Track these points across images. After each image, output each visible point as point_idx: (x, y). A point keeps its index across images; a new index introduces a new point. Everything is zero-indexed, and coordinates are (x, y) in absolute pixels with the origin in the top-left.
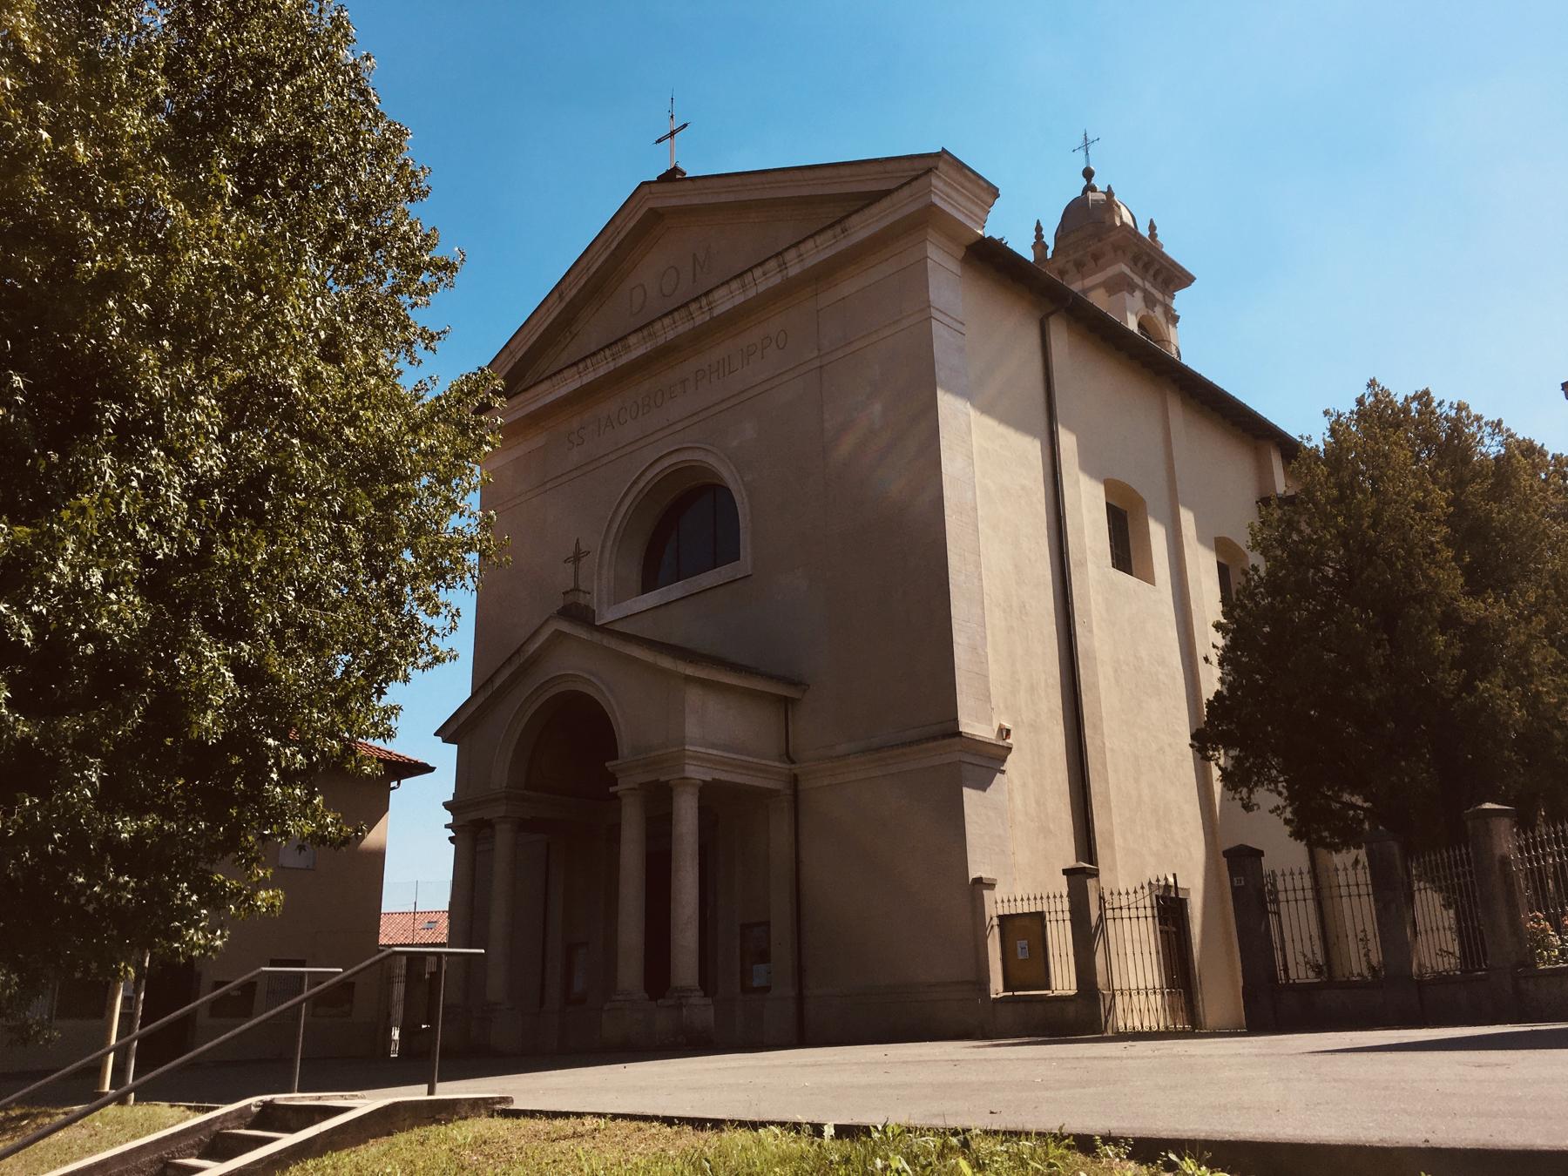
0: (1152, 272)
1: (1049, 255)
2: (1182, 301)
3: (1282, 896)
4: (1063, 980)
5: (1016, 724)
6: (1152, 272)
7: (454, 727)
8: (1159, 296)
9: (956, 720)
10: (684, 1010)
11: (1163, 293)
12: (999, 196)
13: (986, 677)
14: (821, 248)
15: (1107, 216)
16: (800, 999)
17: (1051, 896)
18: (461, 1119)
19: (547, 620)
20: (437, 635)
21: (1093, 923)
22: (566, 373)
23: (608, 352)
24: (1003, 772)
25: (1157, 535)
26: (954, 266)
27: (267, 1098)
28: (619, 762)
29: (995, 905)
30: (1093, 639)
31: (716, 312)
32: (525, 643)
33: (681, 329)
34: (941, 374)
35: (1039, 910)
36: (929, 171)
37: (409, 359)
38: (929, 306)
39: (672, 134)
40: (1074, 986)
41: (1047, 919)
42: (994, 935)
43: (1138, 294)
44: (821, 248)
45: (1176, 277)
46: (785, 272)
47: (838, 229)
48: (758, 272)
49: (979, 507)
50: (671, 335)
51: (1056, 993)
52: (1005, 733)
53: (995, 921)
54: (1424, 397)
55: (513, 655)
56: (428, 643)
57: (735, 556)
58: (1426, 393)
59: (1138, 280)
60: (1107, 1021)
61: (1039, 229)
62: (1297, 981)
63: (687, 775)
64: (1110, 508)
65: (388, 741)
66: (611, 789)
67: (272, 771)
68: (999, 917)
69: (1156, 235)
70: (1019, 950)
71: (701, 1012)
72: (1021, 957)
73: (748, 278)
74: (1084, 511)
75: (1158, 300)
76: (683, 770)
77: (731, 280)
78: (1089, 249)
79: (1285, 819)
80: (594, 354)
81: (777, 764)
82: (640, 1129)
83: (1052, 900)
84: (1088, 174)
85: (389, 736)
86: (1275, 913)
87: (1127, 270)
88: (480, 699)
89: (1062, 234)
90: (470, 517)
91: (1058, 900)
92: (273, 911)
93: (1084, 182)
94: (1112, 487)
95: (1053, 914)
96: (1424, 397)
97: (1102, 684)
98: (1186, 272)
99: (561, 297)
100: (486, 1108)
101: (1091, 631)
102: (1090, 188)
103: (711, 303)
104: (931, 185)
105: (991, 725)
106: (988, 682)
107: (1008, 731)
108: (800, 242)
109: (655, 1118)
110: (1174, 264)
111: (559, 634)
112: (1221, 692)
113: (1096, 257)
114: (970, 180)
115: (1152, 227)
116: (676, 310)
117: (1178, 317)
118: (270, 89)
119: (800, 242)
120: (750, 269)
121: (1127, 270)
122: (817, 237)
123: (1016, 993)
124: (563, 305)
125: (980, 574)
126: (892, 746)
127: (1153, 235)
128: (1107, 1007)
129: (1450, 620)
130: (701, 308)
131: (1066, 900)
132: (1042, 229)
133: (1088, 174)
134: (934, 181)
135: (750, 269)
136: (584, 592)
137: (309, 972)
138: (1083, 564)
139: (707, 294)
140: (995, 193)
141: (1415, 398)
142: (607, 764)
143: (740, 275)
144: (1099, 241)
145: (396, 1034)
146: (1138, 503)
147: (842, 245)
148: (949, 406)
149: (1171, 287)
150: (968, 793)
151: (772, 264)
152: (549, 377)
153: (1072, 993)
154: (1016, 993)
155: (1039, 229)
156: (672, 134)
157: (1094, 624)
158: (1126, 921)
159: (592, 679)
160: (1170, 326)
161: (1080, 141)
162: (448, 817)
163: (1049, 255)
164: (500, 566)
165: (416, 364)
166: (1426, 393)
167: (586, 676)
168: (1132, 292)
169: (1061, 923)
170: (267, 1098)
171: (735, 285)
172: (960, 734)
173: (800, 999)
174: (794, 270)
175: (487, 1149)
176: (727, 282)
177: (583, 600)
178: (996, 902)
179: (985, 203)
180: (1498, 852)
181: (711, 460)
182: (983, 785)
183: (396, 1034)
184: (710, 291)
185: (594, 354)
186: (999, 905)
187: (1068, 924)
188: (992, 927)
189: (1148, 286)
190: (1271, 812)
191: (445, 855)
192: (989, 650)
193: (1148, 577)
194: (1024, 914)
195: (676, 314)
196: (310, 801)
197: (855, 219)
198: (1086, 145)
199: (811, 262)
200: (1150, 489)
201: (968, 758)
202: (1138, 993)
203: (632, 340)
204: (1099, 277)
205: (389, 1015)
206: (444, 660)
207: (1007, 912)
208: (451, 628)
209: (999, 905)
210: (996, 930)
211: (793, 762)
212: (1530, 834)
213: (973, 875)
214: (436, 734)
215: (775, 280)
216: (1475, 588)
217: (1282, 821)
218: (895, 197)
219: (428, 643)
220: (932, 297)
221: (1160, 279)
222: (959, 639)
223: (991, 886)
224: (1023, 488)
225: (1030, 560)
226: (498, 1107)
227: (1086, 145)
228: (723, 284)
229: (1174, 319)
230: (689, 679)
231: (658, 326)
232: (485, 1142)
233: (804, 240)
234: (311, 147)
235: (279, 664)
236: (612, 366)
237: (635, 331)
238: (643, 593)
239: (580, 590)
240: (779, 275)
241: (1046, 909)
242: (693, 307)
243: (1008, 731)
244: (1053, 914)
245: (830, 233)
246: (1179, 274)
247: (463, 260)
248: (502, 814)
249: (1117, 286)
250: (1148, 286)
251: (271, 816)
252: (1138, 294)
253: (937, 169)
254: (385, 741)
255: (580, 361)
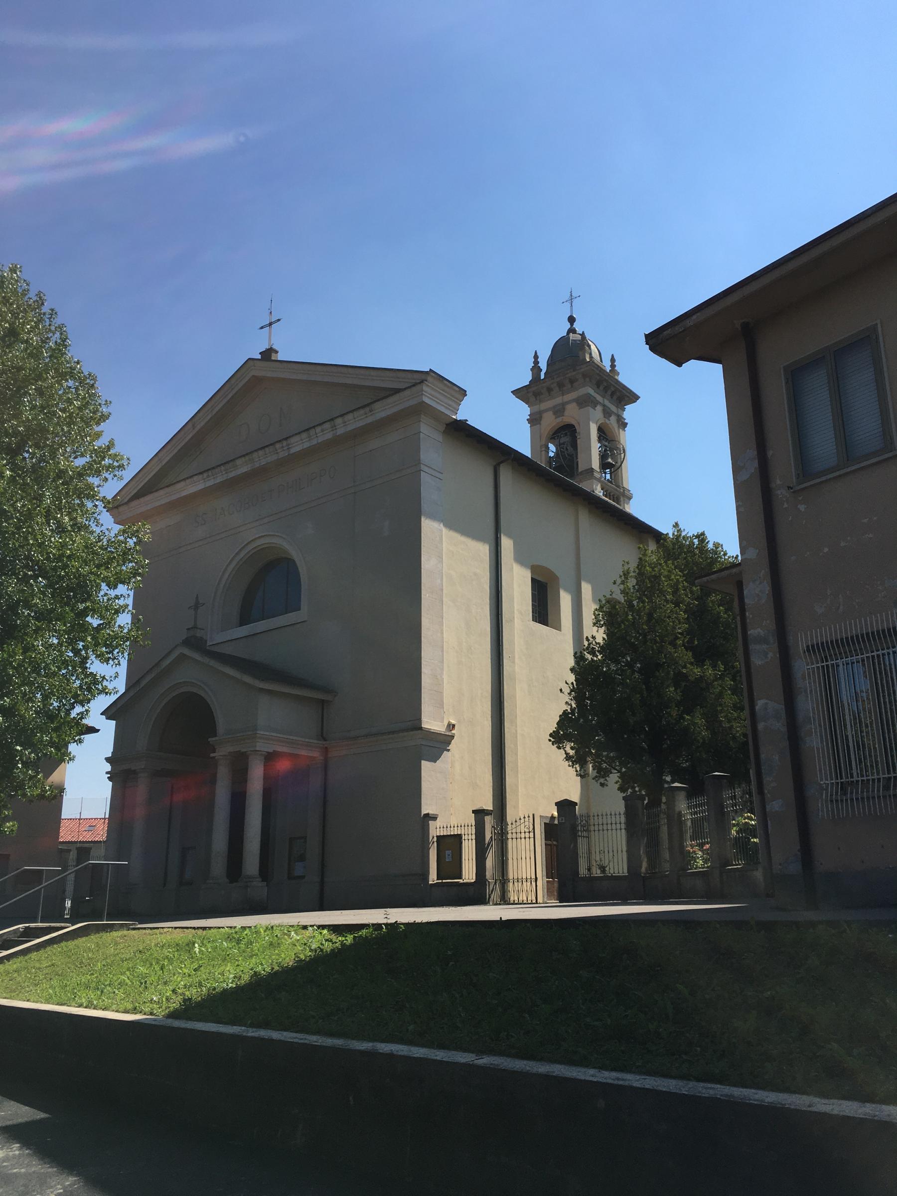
0: (609, 393)
1: (542, 377)
2: (630, 412)
3: (592, 828)
4: (469, 874)
5: (459, 722)
6: (609, 393)
7: (114, 710)
8: (613, 408)
9: (420, 719)
10: (249, 890)
11: (617, 407)
12: (466, 395)
13: (442, 693)
14: (356, 419)
15: (580, 353)
16: (322, 883)
17: (466, 825)
18: (115, 931)
19: (176, 647)
20: (107, 681)
21: (487, 842)
22: (195, 478)
23: (223, 468)
24: (449, 750)
25: (565, 600)
26: (439, 437)
27: (27, 925)
28: (217, 738)
29: (436, 829)
30: (514, 666)
31: (292, 451)
32: (161, 660)
33: (269, 459)
34: (425, 506)
35: (459, 833)
36: (422, 382)
37: (95, 523)
38: (420, 463)
39: (270, 324)
40: (474, 877)
41: (463, 838)
42: (434, 847)
43: (599, 408)
44: (356, 419)
45: (626, 397)
46: (334, 432)
47: (367, 409)
48: (318, 429)
49: (444, 587)
50: (263, 462)
51: (465, 881)
52: (451, 727)
53: (435, 839)
54: (701, 537)
55: (153, 667)
56: (102, 685)
57: (298, 608)
58: (703, 534)
59: (599, 398)
60: (490, 897)
61: (536, 357)
62: (614, 875)
63: (258, 749)
64: (533, 580)
65: (79, 745)
66: (212, 755)
67: (18, 763)
68: (437, 836)
69: (615, 366)
70: (447, 856)
71: (259, 890)
72: (447, 860)
73: (312, 432)
74: (515, 586)
75: (613, 412)
76: (256, 746)
77: (302, 432)
78: (567, 376)
79: (601, 783)
80: (213, 468)
81: (315, 741)
82: (184, 931)
83: (466, 827)
84: (572, 320)
85: (80, 742)
86: (586, 837)
87: (591, 391)
88: (131, 694)
89: (551, 362)
90: (128, 613)
91: (470, 827)
92: (13, 834)
93: (569, 326)
94: (534, 569)
95: (466, 836)
96: (701, 537)
97: (519, 694)
98: (633, 393)
99: (194, 426)
100: (126, 927)
101: (514, 662)
102: (572, 330)
103: (289, 445)
104: (422, 391)
105: (442, 721)
106: (442, 697)
107: (454, 726)
108: (344, 414)
109: (191, 928)
110: (624, 387)
111: (183, 657)
112: (567, 710)
113: (572, 382)
114: (448, 387)
115: (613, 360)
116: (267, 446)
117: (627, 424)
118: (26, 400)
119: (344, 414)
120: (314, 427)
121: (591, 391)
122: (355, 413)
123: (444, 881)
124: (195, 432)
125: (442, 630)
126: (383, 733)
127: (613, 366)
128: (491, 888)
129: (679, 678)
130: (283, 447)
131: (474, 827)
132: (538, 357)
133: (572, 320)
134: (425, 388)
135: (314, 427)
136: (200, 629)
137: (46, 869)
138: (512, 620)
139: (286, 439)
140: (464, 393)
141: (698, 536)
142: (209, 740)
143: (308, 430)
144: (574, 371)
145: (68, 904)
146: (554, 578)
147: (370, 420)
148: (430, 528)
149: (623, 403)
150: (425, 764)
151: (327, 425)
152: (184, 480)
153: (473, 881)
154: (444, 881)
155: (536, 357)
156: (270, 324)
157: (517, 657)
158: (614, 831)
159: (202, 685)
160: (621, 430)
161: (568, 297)
162: (108, 767)
163: (542, 377)
164: (144, 647)
165: (100, 526)
166: (703, 534)
167: (199, 683)
168: (594, 407)
169: (470, 841)
170: (27, 925)
171: (304, 435)
172: (421, 728)
173: (322, 883)
174: (340, 431)
175: (126, 938)
176: (299, 433)
177: (199, 634)
178: (436, 828)
179: (455, 409)
180: (677, 809)
181: (286, 545)
182: (434, 758)
183: (68, 904)
184: (290, 437)
185: (213, 468)
186: (438, 830)
187: (474, 841)
188: (433, 842)
189: (607, 403)
190: (593, 779)
191: (106, 789)
192: (445, 677)
193: (557, 627)
194: (451, 835)
195: (267, 449)
196: (36, 776)
197: (377, 405)
198: (571, 299)
199: (350, 428)
200: (561, 568)
201: (424, 743)
202: (527, 881)
203: (239, 462)
204: (573, 395)
205: (64, 891)
206: (110, 694)
207: (442, 834)
208: (115, 677)
209: (438, 830)
210: (435, 844)
211: (325, 740)
212: (697, 799)
213: (424, 812)
214: (102, 714)
215: (329, 436)
216: (699, 661)
217: (599, 784)
218: (402, 394)
219: (102, 685)
220: (422, 457)
221: (615, 397)
222: (426, 670)
223: (434, 818)
224: (475, 574)
225: (476, 619)
226: (131, 927)
227: (571, 299)
228: (296, 434)
229: (624, 425)
230: (261, 690)
231: (255, 455)
232: (125, 936)
233: (348, 413)
234: (48, 431)
235: (25, 709)
236: (225, 477)
237: (241, 457)
238: (241, 626)
239: (197, 628)
240: (332, 433)
241: (463, 833)
242: (278, 446)
243: (454, 726)
244: (466, 836)
245: (362, 412)
246: (628, 394)
247: (129, 463)
248: (143, 767)
249: (585, 402)
250: (607, 403)
251: (17, 786)
252: (599, 408)
253: (426, 381)
254: (77, 744)
255: (204, 472)
